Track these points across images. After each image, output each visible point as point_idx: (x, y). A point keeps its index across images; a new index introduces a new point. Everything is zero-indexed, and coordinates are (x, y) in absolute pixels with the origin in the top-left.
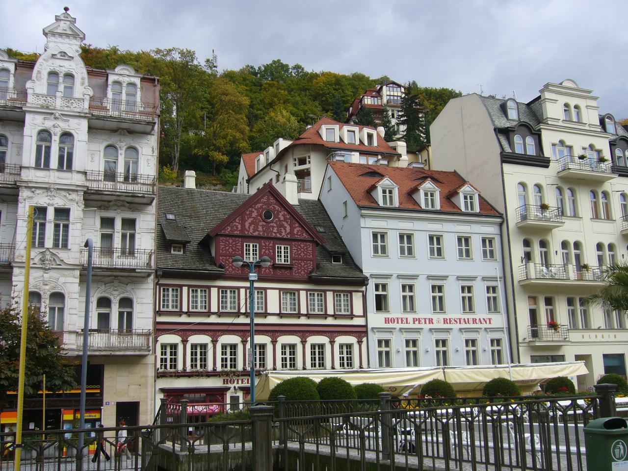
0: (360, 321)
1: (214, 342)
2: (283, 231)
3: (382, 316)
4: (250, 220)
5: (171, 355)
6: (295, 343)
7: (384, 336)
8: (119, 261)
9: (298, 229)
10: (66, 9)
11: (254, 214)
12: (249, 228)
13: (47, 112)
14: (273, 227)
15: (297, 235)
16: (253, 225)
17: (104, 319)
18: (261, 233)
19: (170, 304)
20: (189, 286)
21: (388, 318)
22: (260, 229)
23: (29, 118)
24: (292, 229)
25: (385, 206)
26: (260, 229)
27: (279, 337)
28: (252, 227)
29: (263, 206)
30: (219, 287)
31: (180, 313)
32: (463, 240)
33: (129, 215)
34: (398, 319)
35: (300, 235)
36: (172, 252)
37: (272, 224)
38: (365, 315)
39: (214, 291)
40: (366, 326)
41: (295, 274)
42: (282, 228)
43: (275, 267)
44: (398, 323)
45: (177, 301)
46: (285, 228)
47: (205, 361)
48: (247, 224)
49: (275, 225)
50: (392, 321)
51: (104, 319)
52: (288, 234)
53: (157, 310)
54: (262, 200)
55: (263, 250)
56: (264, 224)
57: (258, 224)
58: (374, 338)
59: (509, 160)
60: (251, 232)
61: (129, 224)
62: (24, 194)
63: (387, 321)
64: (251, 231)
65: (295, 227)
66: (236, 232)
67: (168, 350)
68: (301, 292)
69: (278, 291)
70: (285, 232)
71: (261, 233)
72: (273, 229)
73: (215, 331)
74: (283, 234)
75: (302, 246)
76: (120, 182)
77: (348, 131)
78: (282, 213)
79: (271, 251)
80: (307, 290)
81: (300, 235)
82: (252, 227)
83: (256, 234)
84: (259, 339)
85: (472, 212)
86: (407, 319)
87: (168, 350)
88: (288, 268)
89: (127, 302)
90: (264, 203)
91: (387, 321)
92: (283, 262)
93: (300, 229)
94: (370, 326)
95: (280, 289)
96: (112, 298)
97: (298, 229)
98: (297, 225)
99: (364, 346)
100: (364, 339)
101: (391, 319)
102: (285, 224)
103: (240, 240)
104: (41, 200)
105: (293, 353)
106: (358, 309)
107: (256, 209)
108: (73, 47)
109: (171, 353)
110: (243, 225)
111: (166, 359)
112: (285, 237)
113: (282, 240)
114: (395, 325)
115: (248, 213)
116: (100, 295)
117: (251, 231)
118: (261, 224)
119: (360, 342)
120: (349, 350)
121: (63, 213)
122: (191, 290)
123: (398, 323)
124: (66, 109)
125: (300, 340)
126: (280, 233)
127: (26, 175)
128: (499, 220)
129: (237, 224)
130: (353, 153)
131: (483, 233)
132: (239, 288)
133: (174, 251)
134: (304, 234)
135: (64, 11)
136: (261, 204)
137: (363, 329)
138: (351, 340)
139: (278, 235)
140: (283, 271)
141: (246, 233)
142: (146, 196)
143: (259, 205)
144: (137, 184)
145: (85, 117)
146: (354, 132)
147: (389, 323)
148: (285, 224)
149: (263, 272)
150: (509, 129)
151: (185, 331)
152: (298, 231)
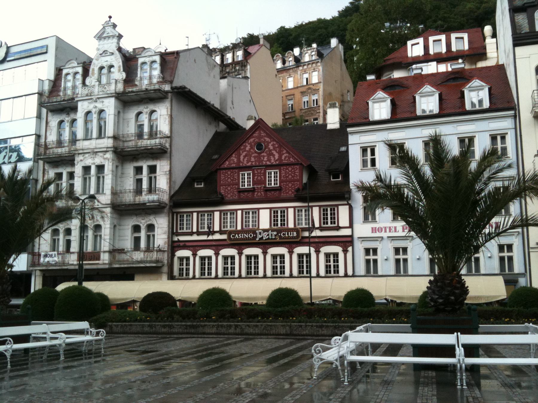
0: (348, 232)
1: (240, 254)
2: (272, 158)
3: (369, 226)
4: (244, 154)
5: (334, 262)
6: (188, 256)
7: (371, 245)
8: (145, 198)
9: (285, 155)
10: (110, 17)
11: (248, 148)
12: (243, 160)
13: (89, 97)
14: (264, 156)
15: (285, 160)
16: (246, 158)
17: (137, 240)
18: (253, 163)
19: (304, 222)
20: (198, 212)
21: (375, 228)
22: (253, 159)
23: (80, 104)
24: (280, 156)
25: (474, 109)
26: (253, 159)
27: (269, 248)
28: (246, 159)
29: (255, 140)
30: (221, 211)
31: (192, 234)
32: (499, 138)
33: (151, 163)
34: (385, 228)
35: (287, 160)
36: (196, 186)
37: (263, 154)
38: (351, 226)
39: (217, 214)
40: (351, 236)
41: (283, 195)
42: (271, 157)
43: (267, 190)
44: (386, 231)
45: (298, 220)
46: (274, 156)
47: (248, 267)
48: (242, 158)
49: (265, 154)
50: (380, 230)
51: (137, 240)
52: (277, 160)
53: (175, 231)
54: (254, 135)
55: (256, 177)
56: (256, 155)
57: (251, 156)
58: (359, 247)
59: (521, 42)
60: (245, 163)
61: (152, 169)
62: (78, 159)
63: (374, 230)
64: (245, 162)
65: (283, 154)
66: (233, 165)
67: (278, 259)
68: (314, 208)
69: (268, 210)
70: (274, 159)
71: (253, 163)
72: (264, 158)
73: (217, 246)
74: (272, 161)
75: (290, 169)
76: (146, 139)
77: (456, 38)
78: (272, 143)
79: (262, 177)
80: (294, 207)
81: (287, 160)
82: (246, 159)
83: (249, 164)
84: (304, 250)
85: (481, 108)
86: (395, 228)
87: (278, 259)
88: (279, 189)
89: (151, 228)
90: (256, 137)
91: (374, 230)
92: (246, 186)
93: (287, 155)
94: (356, 236)
95: (270, 209)
96: (141, 225)
97: (285, 155)
98: (285, 152)
99: (349, 255)
100: (350, 249)
101: (379, 228)
102: (274, 152)
103: (237, 171)
104: (88, 161)
105: (336, 261)
106: (344, 220)
107: (249, 144)
108: (111, 45)
109: (334, 260)
110: (239, 159)
111: (330, 266)
112: (274, 163)
113: (272, 167)
114: (383, 234)
115: (242, 148)
116: (133, 224)
117: (245, 162)
118: (253, 155)
119: (345, 251)
120: (336, 259)
121: (100, 168)
122: (200, 215)
123: (386, 231)
124: (101, 93)
125: (262, 251)
126: (269, 160)
127: (81, 145)
128: (512, 112)
129: (234, 158)
130: (430, 63)
131: (493, 129)
132: (236, 210)
133: (197, 185)
134: (291, 159)
135: (109, 19)
136: (253, 139)
137: (349, 239)
138: (337, 249)
139: (268, 163)
140: (273, 192)
141: (241, 164)
142: (154, 147)
143: (252, 140)
144: (64, 147)
145: (112, 97)
146: (462, 38)
147: (376, 232)
148: (274, 152)
149: (255, 196)
150: (526, 5)
151: (195, 247)
152: (286, 157)
